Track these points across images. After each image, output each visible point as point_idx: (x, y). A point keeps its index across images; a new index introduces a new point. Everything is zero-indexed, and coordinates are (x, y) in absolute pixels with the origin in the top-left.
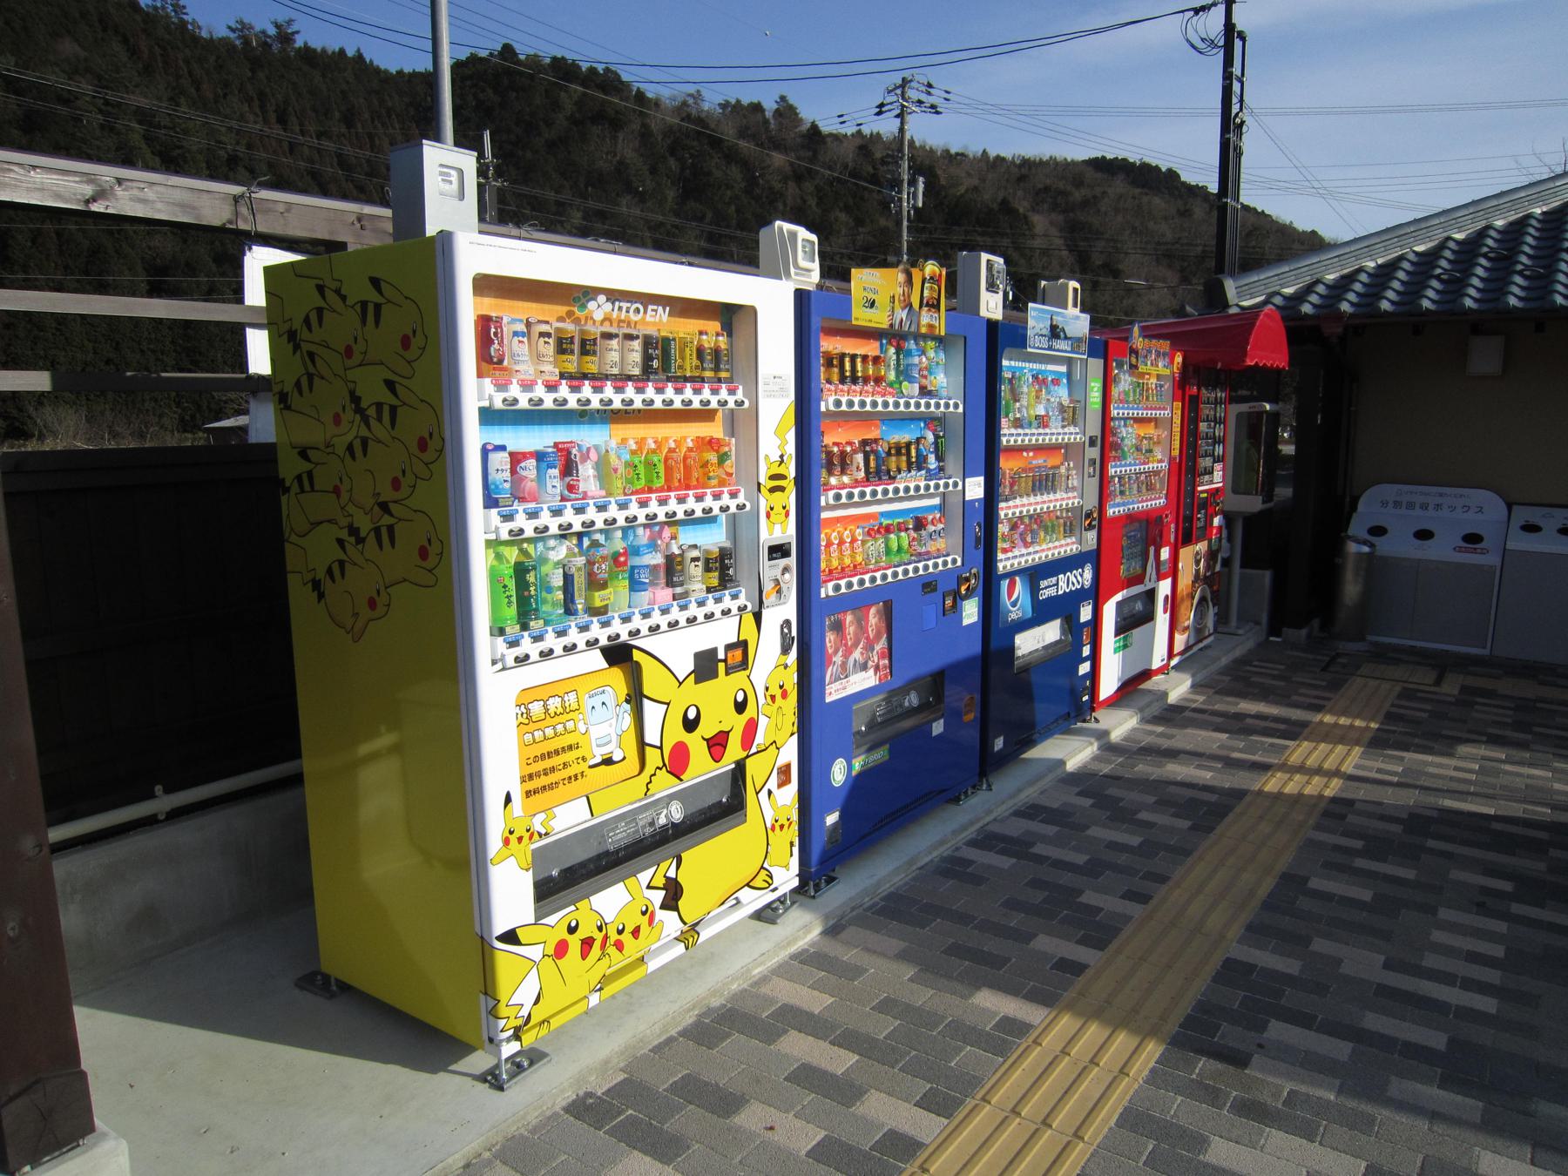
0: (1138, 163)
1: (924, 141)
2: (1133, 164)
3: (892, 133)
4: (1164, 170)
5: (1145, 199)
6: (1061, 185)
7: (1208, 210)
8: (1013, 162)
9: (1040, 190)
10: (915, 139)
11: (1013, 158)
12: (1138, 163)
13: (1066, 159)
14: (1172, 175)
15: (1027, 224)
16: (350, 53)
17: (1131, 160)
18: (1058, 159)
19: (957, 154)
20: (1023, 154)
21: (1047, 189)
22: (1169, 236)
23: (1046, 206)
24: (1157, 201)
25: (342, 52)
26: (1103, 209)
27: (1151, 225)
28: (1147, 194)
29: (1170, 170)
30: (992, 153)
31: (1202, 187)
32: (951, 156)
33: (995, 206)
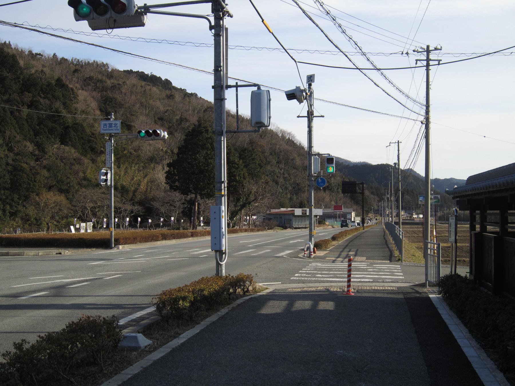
0: (150, 75)
1: (17, 45)
2: (147, 75)
3: (2, 40)
4: (163, 79)
5: (148, 88)
6: (100, 77)
7: (183, 97)
8: (72, 63)
9: (87, 78)
10: (11, 43)
11: (72, 60)
12: (150, 75)
13: (103, 63)
14: (131, 71)
15: (73, 94)
16: (7, 42)
17: (146, 73)
18: (99, 63)
19: (37, 54)
20: (78, 58)
21: (90, 78)
22: (162, 109)
23: (90, 87)
24: (154, 89)
25: (5, 42)
26: (123, 91)
27: (151, 102)
28: (149, 85)
29: (166, 80)
30: (60, 56)
31: (184, 90)
32: (33, 54)
33: (53, 82)
